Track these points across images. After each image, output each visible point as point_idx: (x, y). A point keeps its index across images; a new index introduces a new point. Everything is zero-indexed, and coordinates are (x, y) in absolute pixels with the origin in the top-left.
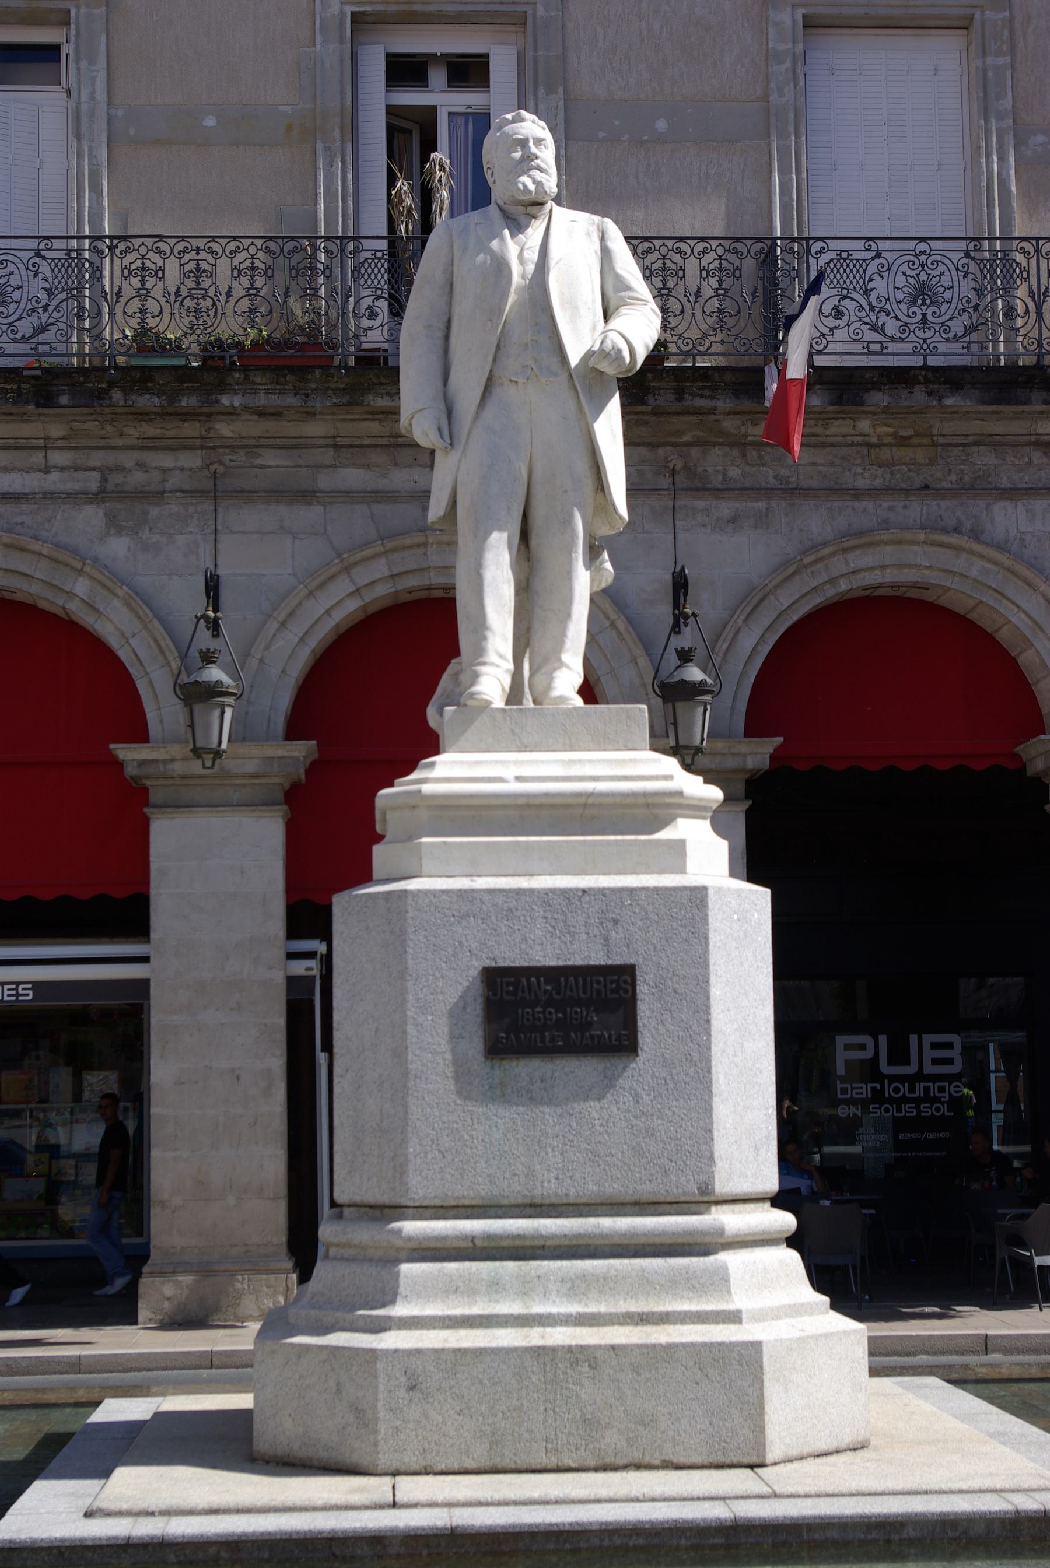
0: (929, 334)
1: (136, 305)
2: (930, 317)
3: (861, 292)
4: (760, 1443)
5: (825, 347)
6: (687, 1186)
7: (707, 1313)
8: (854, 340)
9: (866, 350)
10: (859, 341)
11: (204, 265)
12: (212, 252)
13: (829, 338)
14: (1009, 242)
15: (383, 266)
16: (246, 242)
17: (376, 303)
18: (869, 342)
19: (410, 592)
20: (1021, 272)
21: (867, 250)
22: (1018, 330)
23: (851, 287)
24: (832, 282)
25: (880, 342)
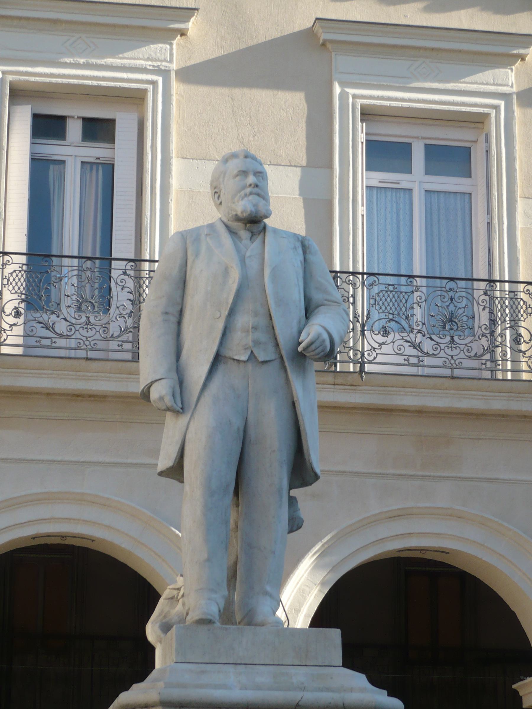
0: (455, 352)
2: (456, 338)
3: (404, 317)
5: (375, 358)
8: (398, 354)
9: (406, 362)
10: (401, 355)
13: (378, 351)
14: (516, 284)
15: (22, 276)
17: (388, 324)
18: (409, 356)
19: (34, 538)
20: (527, 308)
21: (408, 285)
22: (524, 352)
23: (396, 313)
24: (14, 288)
25: (418, 357)
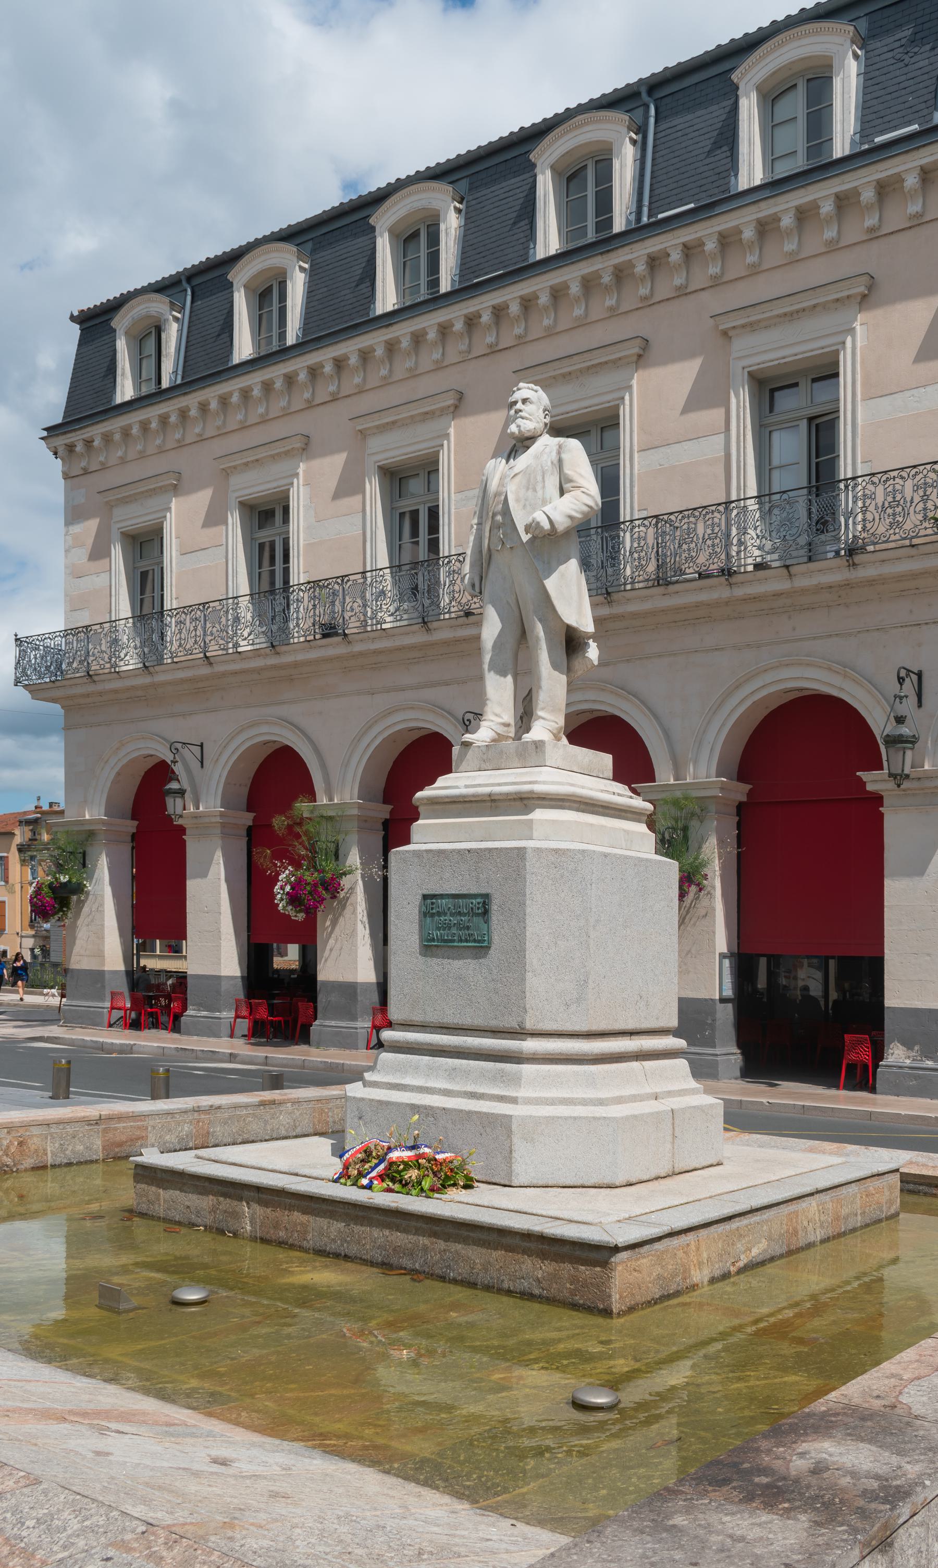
1: (921, 505)
4: (510, 1173)
6: (511, 1022)
7: (547, 1099)
11: (898, 487)
12: (902, 478)
16: (921, 468)
